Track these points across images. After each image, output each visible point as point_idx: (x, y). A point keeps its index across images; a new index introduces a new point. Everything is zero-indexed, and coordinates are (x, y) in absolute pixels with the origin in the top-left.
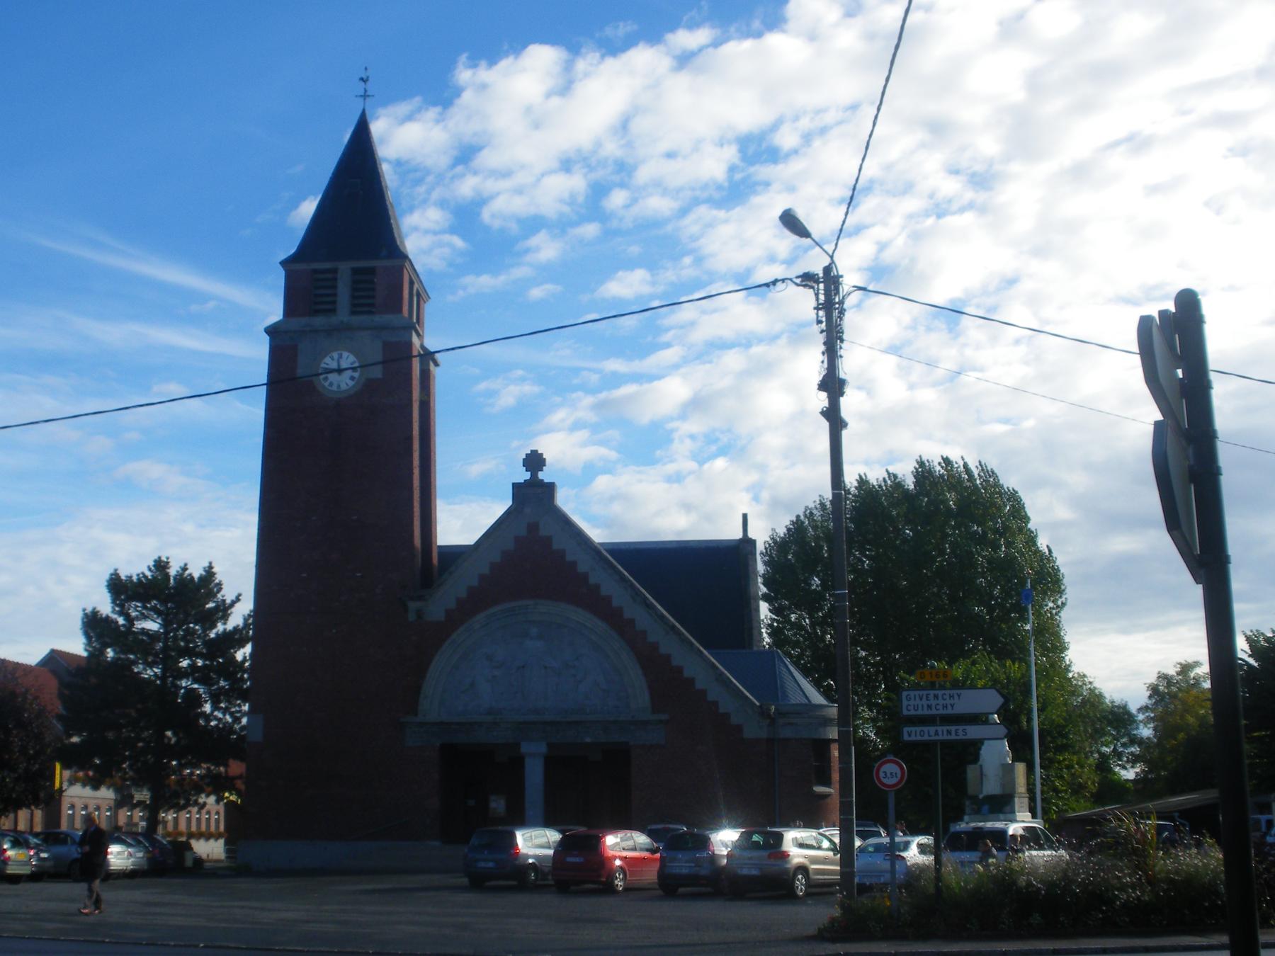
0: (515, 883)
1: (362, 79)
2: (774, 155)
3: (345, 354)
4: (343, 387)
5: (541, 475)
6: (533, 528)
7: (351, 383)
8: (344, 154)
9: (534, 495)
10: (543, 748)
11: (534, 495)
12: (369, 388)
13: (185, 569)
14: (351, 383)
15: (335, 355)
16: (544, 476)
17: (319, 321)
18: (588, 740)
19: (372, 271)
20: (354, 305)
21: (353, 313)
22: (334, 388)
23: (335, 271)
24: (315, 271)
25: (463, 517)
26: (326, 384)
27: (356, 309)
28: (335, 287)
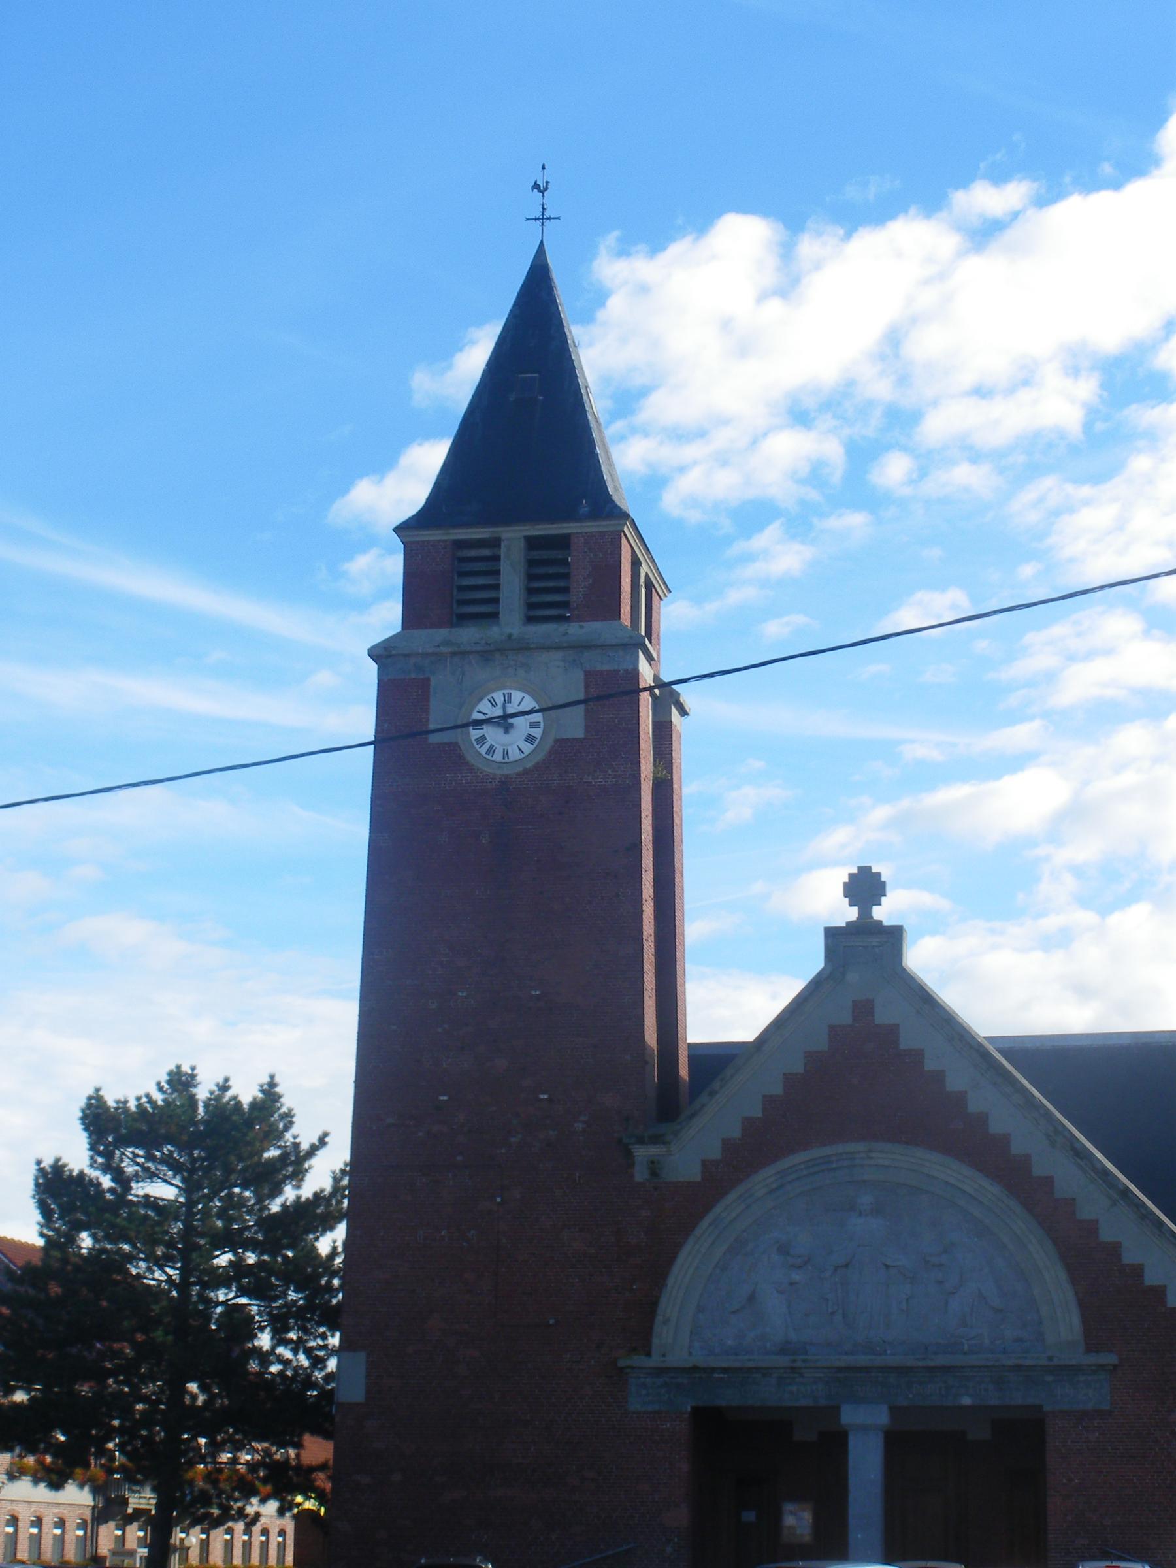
4: (514, 755)
5: (878, 913)
6: (863, 1009)
7: (528, 748)
9: (864, 950)
10: (881, 1416)
11: (864, 950)
14: (528, 748)
15: (499, 697)
17: (468, 635)
18: (966, 1401)
19: (564, 542)
20: (531, 606)
21: (530, 620)
22: (498, 757)
23: (495, 543)
24: (459, 544)
26: (483, 750)
27: (534, 613)
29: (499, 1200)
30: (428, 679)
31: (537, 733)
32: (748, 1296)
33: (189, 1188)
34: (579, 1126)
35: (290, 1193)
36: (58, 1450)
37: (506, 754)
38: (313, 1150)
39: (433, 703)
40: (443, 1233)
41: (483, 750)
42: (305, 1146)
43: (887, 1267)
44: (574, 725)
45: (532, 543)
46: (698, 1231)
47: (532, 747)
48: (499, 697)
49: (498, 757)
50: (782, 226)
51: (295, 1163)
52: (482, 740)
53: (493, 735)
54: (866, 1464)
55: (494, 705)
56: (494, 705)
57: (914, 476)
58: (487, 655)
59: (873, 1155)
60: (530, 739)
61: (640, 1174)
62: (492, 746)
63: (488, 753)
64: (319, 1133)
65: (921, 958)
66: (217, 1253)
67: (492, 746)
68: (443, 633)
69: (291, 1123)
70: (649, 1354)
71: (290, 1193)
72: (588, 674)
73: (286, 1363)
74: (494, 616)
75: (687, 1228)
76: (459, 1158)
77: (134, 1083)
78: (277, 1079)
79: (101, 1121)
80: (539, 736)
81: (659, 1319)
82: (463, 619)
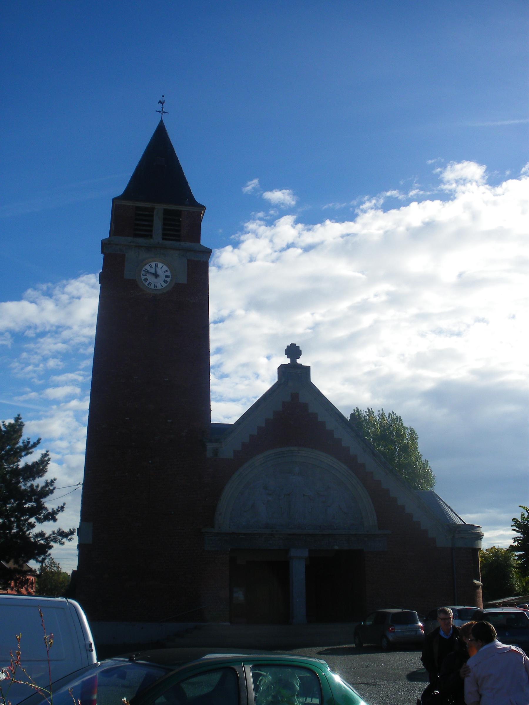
0: (354, 645)
1: (160, 102)
2: (27, 340)
3: (160, 265)
4: (159, 287)
5: (299, 361)
6: (295, 396)
7: (164, 285)
8: (150, 142)
9: (294, 376)
10: (306, 553)
11: (294, 376)
12: (177, 289)
14: (164, 285)
15: (153, 264)
16: (302, 361)
17: (140, 241)
18: (336, 548)
19: (178, 213)
20: (164, 234)
21: (163, 239)
22: (152, 287)
23: (153, 209)
24: (138, 208)
25: (235, 389)
26: (146, 284)
27: (165, 237)
28: (152, 221)
29: (150, 462)
30: (125, 255)
31: (168, 279)
32: (248, 503)
37: (155, 286)
40: (126, 474)
41: (146, 284)
43: (304, 495)
44: (183, 280)
47: (166, 285)
48: (153, 264)
49: (152, 287)
52: (146, 280)
53: (151, 279)
54: (298, 571)
55: (151, 267)
56: (151, 267)
57: (49, 335)
58: (148, 249)
59: (300, 452)
60: (165, 281)
61: (209, 454)
62: (150, 282)
63: (148, 284)
64: (37, 439)
65: (316, 379)
67: (150, 282)
68: (130, 239)
72: (189, 261)
74: (151, 236)
76: (133, 444)
78: (21, 416)
80: (169, 281)
82: (136, 236)
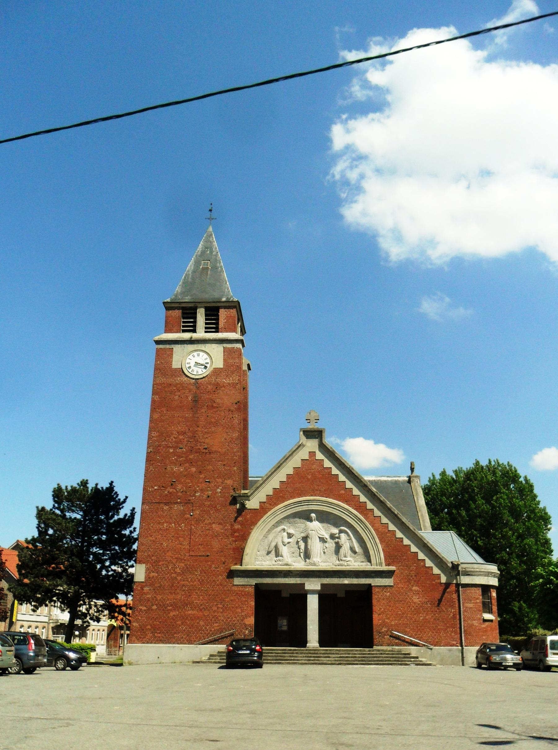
13: (97, 485)
17: (187, 336)
21: (206, 332)
33: (84, 517)
34: (219, 490)
35: (116, 518)
36: (34, 606)
38: (124, 501)
39: (174, 356)
42: (122, 500)
45: (194, 331)
46: (258, 525)
50: (410, 32)
51: (119, 505)
58: (191, 342)
66: (510, 658)
69: (118, 495)
70: (241, 565)
71: (116, 518)
73: (114, 571)
75: (254, 523)
77: (70, 481)
79: (58, 494)
81: (245, 553)
